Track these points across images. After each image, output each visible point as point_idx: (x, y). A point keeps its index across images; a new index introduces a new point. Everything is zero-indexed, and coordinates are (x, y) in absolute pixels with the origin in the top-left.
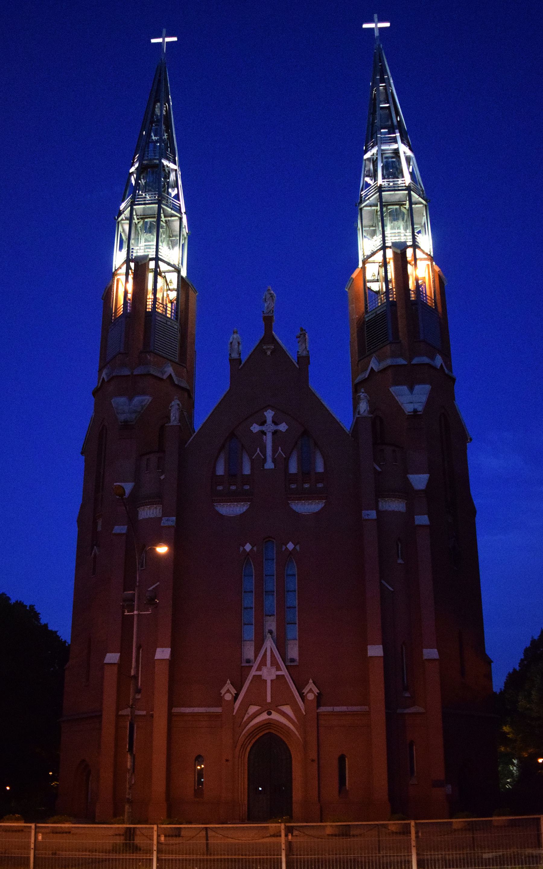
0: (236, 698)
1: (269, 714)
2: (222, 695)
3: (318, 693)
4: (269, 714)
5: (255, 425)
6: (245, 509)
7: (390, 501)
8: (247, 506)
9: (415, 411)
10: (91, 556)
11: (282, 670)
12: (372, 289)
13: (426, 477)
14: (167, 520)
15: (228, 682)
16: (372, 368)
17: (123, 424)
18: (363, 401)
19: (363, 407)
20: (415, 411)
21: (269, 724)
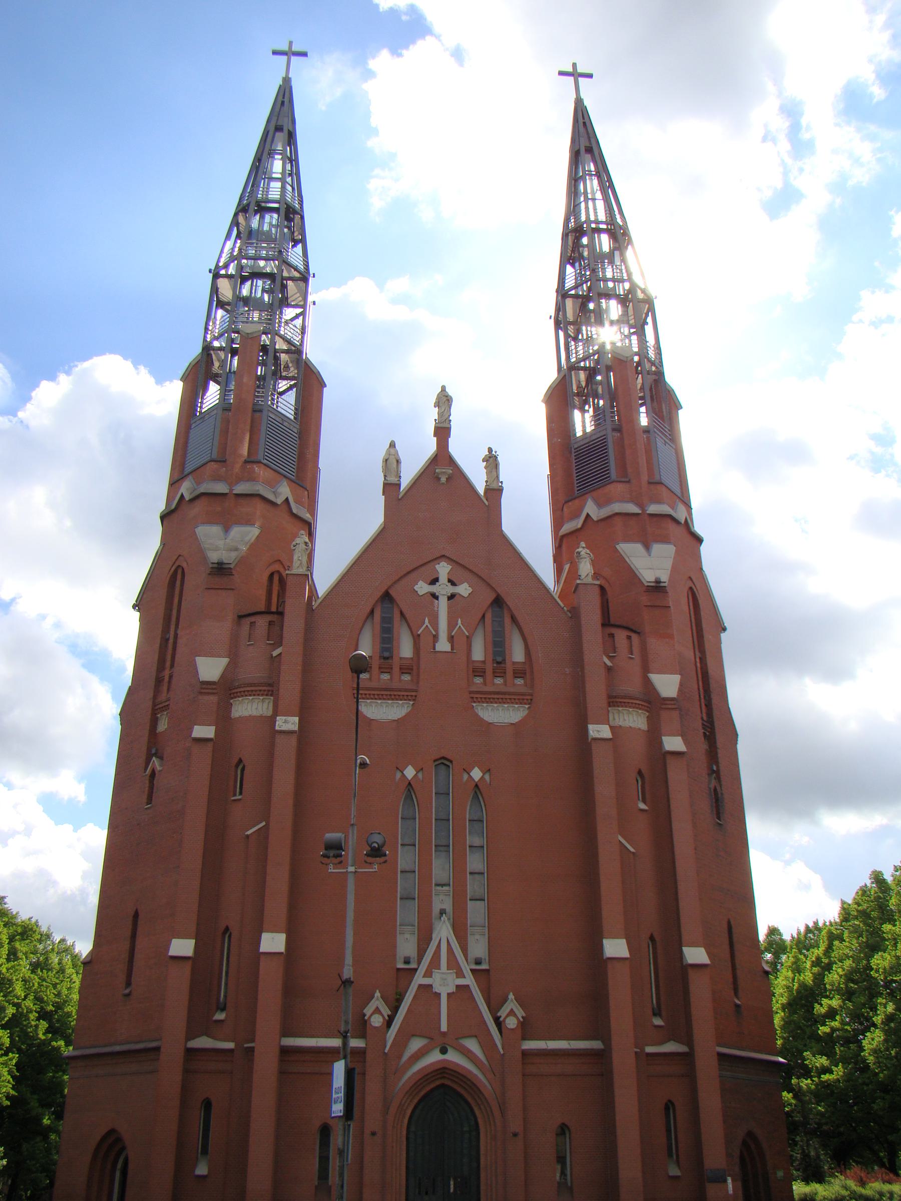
0: (389, 1023)
1: (444, 1051)
2: (366, 1018)
4: (444, 1051)
5: (421, 583)
7: (634, 713)
8: (408, 707)
9: (658, 581)
10: (145, 772)
11: (465, 978)
14: (286, 722)
15: (376, 995)
16: (588, 515)
17: (216, 566)
18: (584, 560)
19: (586, 569)
20: (658, 581)
21: (444, 1071)
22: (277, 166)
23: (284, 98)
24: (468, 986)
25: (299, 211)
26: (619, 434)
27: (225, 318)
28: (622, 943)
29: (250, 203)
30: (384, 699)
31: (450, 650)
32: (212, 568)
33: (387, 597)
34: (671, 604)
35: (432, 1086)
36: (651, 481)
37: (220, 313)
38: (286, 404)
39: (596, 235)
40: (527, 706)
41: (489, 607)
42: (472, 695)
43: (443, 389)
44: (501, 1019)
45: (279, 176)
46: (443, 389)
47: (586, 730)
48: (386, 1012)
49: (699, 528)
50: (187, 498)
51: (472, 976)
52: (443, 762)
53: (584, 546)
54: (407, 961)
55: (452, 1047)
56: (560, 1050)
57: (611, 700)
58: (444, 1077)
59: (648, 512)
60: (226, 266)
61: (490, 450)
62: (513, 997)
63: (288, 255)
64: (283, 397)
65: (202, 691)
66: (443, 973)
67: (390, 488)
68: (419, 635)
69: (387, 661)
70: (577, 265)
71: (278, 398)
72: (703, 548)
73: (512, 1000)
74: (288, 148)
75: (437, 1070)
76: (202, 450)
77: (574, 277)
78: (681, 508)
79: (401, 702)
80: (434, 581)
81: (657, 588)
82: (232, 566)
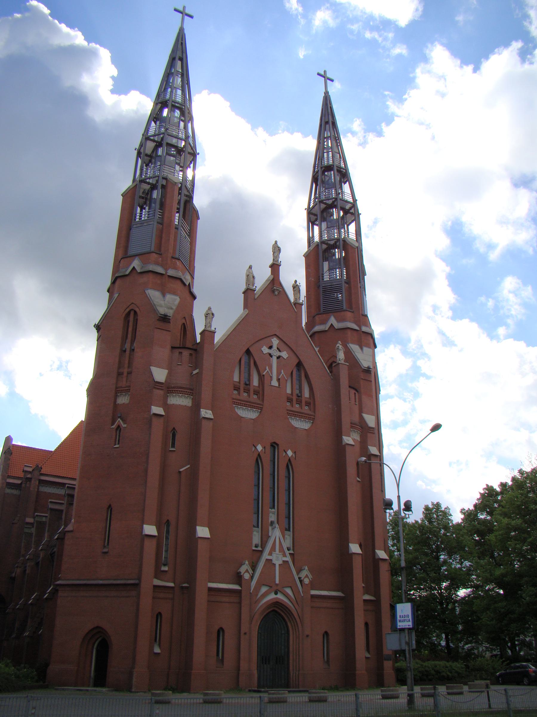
0: (252, 577)
1: (276, 593)
4: (276, 593)
9: (369, 368)
12: (365, 277)
16: (134, 268)
21: (277, 604)
23: (182, 41)
26: (347, 285)
28: (206, 530)
30: (247, 407)
31: (278, 386)
32: (160, 317)
33: (248, 352)
36: (173, 256)
40: (312, 421)
44: (302, 579)
46: (276, 242)
47: (341, 440)
48: (251, 571)
49: (196, 290)
51: (289, 557)
52: (274, 445)
53: (341, 343)
54: (256, 546)
55: (280, 592)
56: (334, 596)
62: (248, 563)
65: (156, 387)
66: (277, 554)
67: (248, 292)
68: (264, 375)
70: (158, 123)
72: (195, 302)
75: (272, 603)
76: (142, 243)
77: (154, 130)
78: (188, 277)
82: (170, 318)
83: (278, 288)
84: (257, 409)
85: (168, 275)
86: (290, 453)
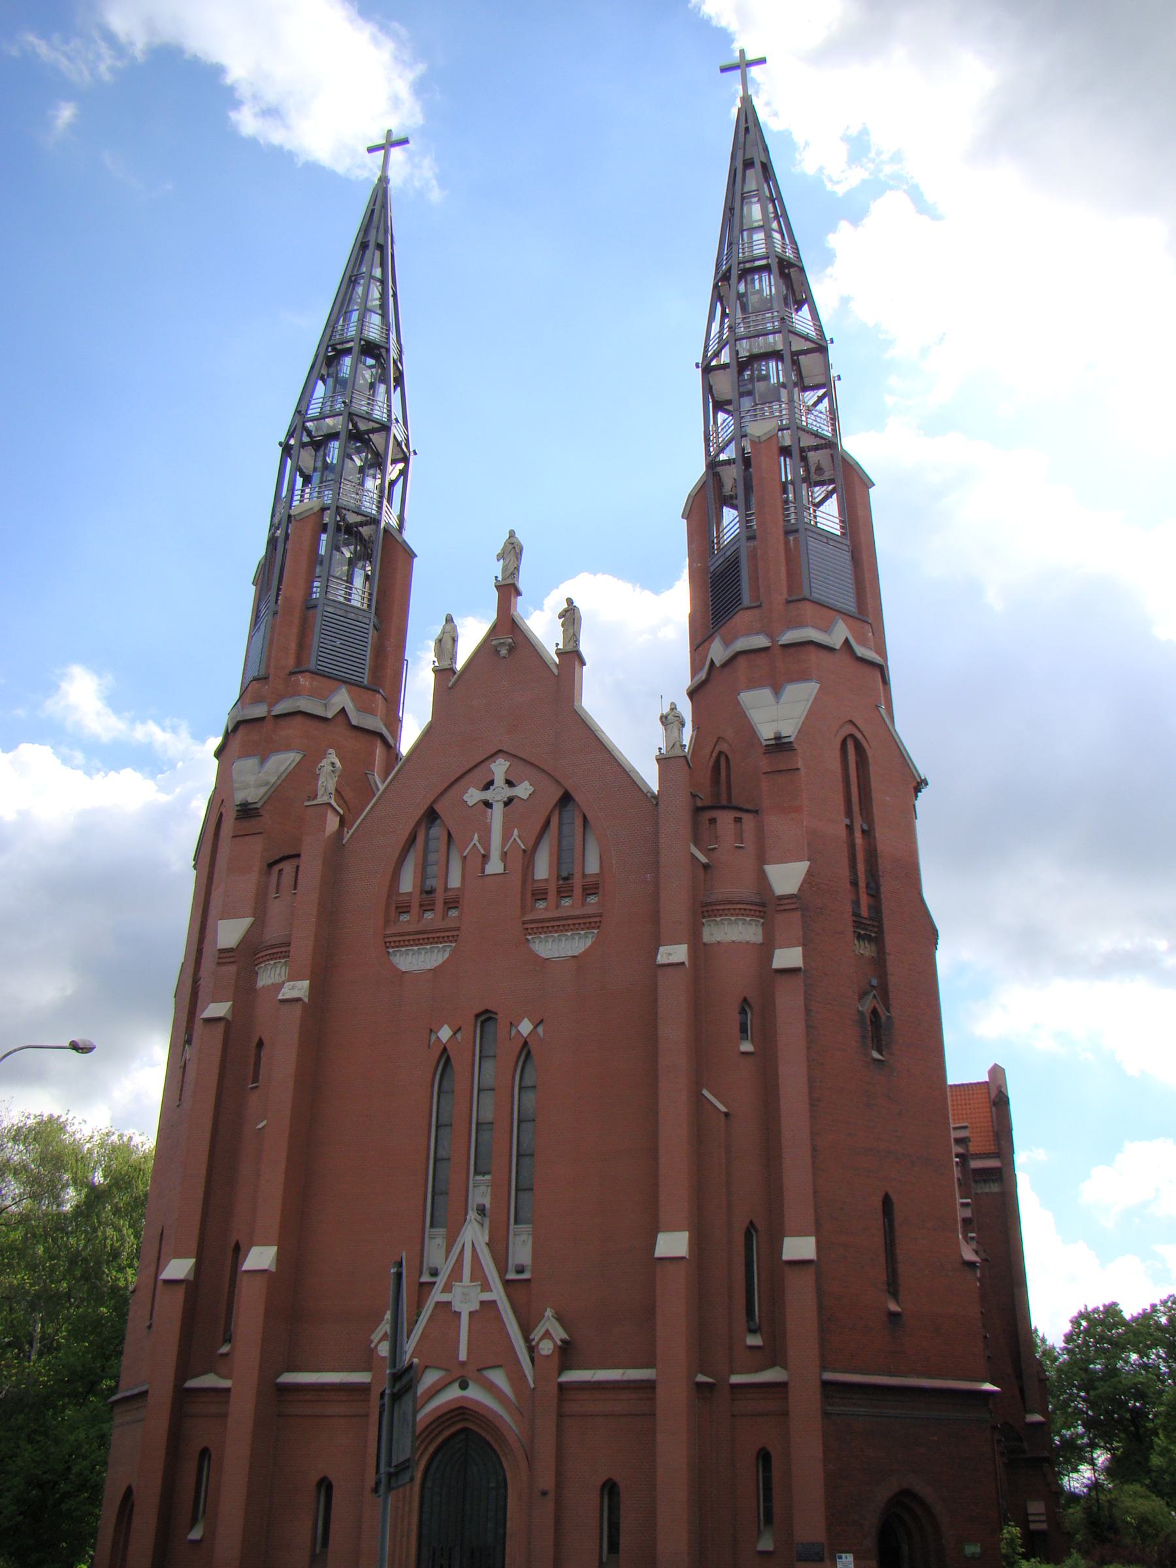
1: (464, 1386)
2: (373, 1345)
3: (562, 1340)
4: (464, 1386)
5: (472, 791)
6: (589, 942)
9: (778, 738)
11: (492, 1291)
13: (802, 867)
15: (386, 1317)
20: (778, 738)
21: (461, 1411)
22: (755, 212)
24: (494, 1302)
25: (797, 263)
27: (728, 421)
29: (730, 267)
30: (421, 944)
34: (800, 765)
35: (453, 1429)
37: (721, 416)
38: (828, 517)
39: (756, 277)
41: (556, 805)
42: (526, 926)
43: (512, 534)
44: (534, 1343)
45: (761, 223)
46: (512, 534)
50: (718, 664)
56: (634, 1381)
57: (705, 909)
58: (466, 1419)
59: (780, 643)
60: (717, 354)
61: (570, 601)
63: (793, 322)
64: (820, 509)
66: (464, 1287)
69: (568, 882)
71: (815, 511)
73: (549, 1319)
74: (765, 186)
79: (441, 946)
80: (489, 785)
81: (780, 746)
82: (792, 739)
83: (502, 641)
84: (446, 942)
85: (781, 645)
86: (525, 1027)
